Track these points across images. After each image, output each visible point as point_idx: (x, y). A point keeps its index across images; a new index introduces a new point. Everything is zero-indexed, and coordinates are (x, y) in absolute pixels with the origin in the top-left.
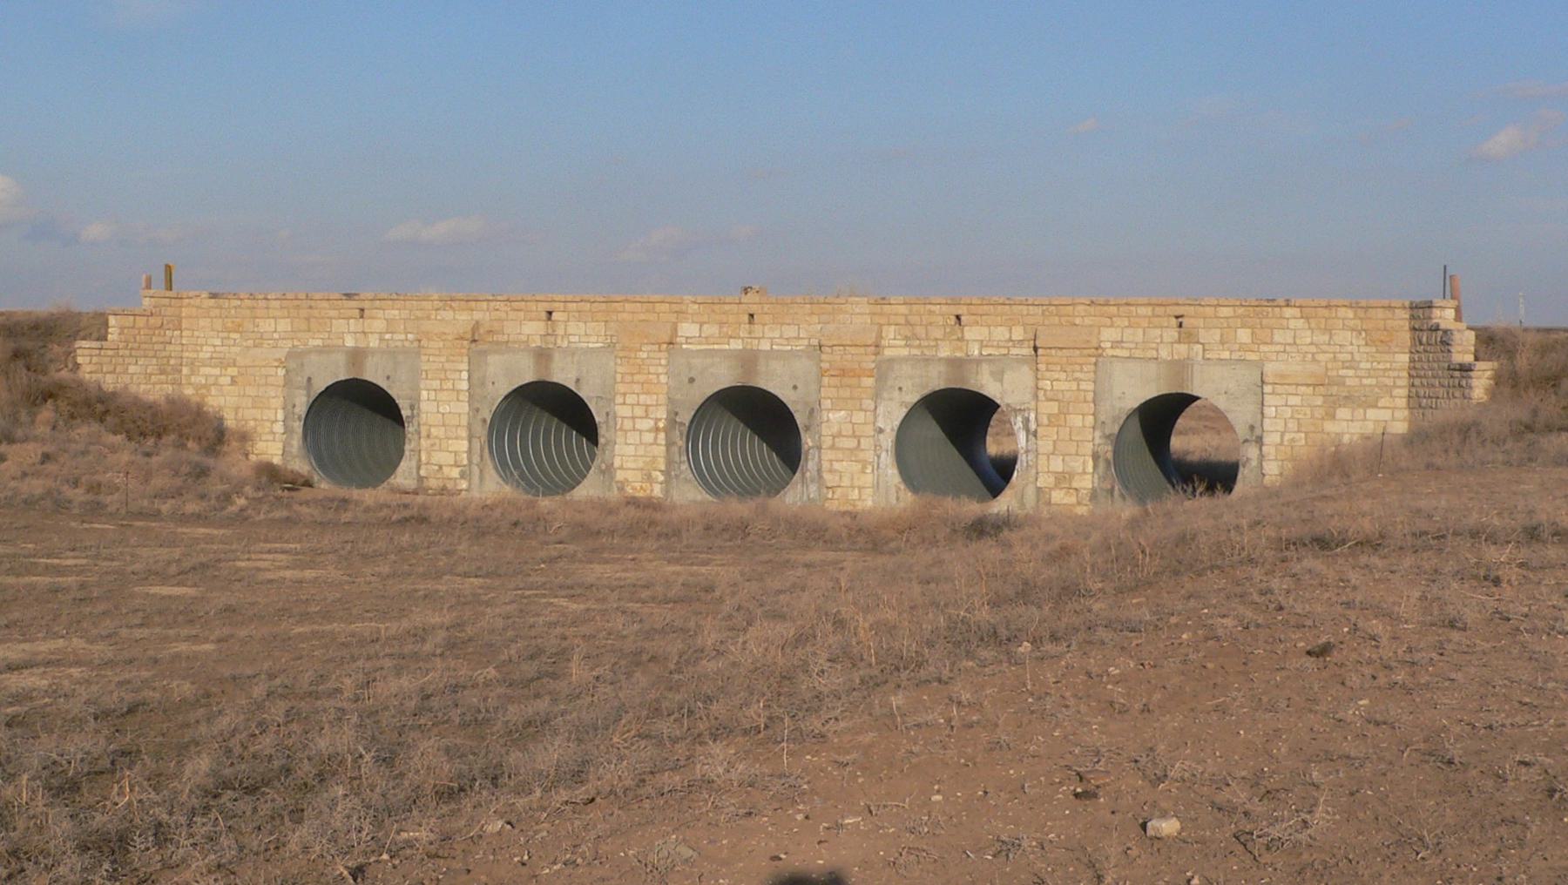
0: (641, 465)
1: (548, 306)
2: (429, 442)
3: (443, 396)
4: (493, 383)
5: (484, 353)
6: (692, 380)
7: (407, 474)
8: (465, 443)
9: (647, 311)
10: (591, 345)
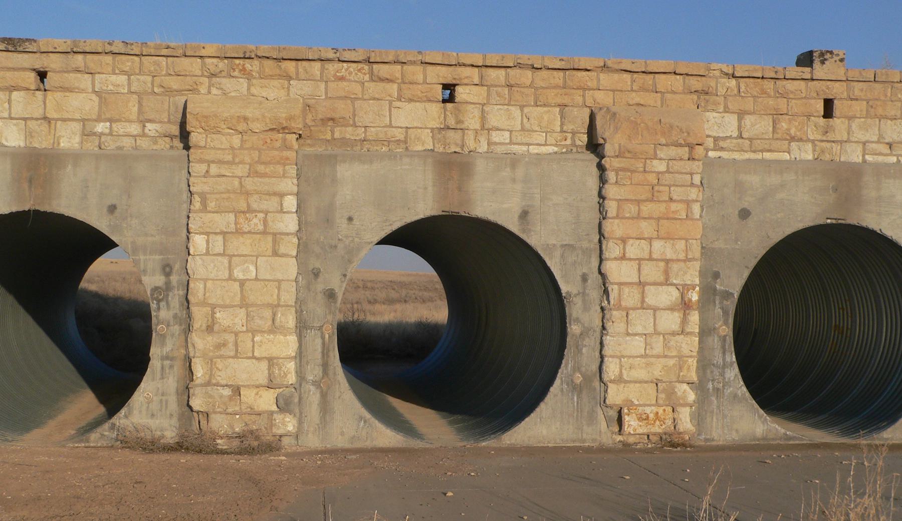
0: (657, 373)
1: (446, 75)
2: (211, 340)
3: (242, 245)
4: (350, 219)
5: (331, 160)
6: (745, 214)
7: (154, 406)
8: (293, 339)
9: (643, 89)
10: (534, 150)
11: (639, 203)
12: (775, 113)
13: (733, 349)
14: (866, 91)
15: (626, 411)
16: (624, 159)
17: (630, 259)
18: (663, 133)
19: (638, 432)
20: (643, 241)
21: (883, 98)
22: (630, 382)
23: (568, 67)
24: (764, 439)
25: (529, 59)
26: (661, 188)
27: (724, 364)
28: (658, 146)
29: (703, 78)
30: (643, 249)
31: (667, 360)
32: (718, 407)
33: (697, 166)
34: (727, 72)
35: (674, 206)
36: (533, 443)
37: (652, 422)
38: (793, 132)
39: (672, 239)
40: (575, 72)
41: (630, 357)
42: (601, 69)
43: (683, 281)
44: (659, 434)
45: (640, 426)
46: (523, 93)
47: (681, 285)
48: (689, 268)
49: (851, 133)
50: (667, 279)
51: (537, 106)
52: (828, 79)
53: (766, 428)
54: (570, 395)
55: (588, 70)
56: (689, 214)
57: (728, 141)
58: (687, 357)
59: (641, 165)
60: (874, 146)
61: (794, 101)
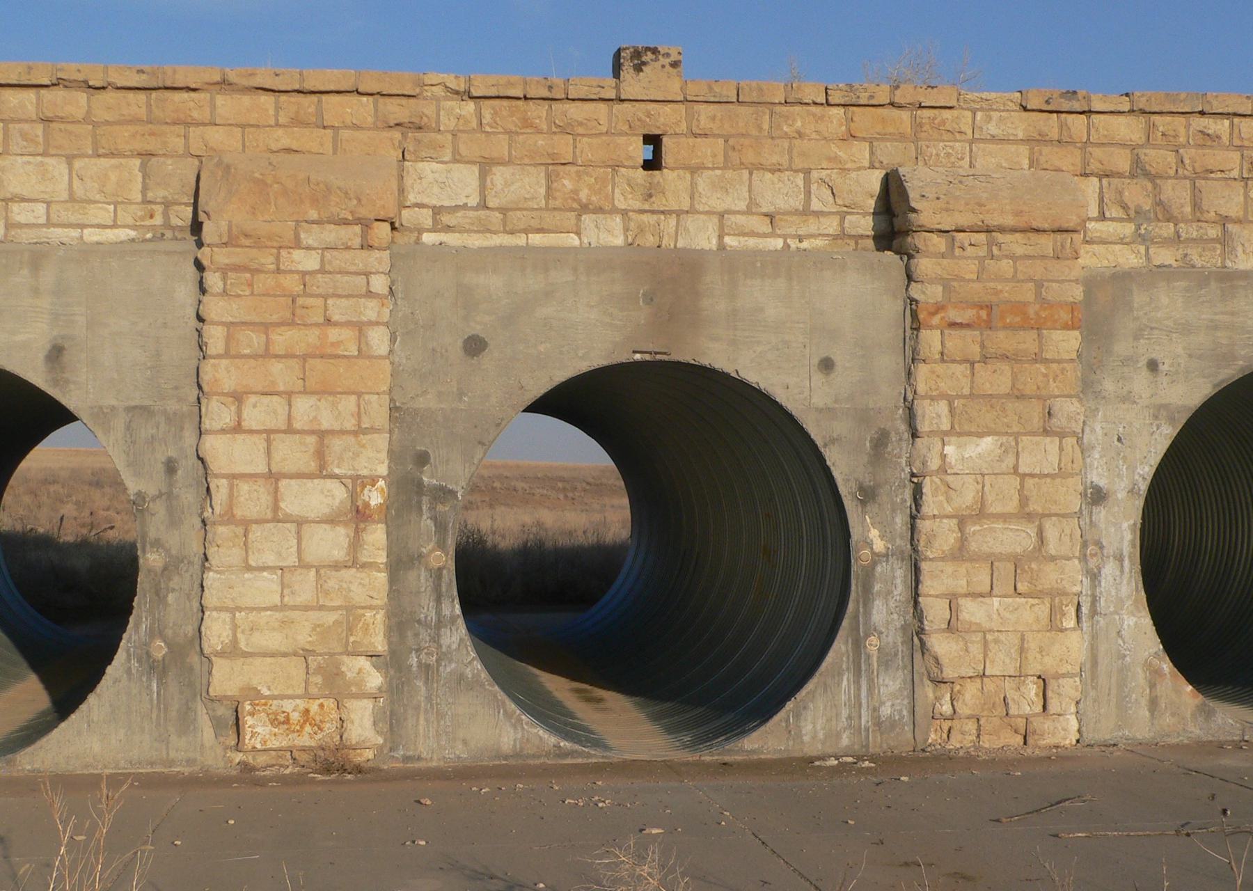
0: (304, 637)
6: (475, 346)
9: (297, 122)
10: (91, 235)
11: (267, 328)
12: (550, 161)
13: (455, 593)
14: (721, 120)
15: (248, 707)
16: (238, 250)
17: (251, 432)
18: (315, 201)
19: (269, 745)
20: (275, 398)
21: (754, 132)
22: (251, 655)
23: (155, 85)
24: (517, 755)
25: (79, 71)
26: (310, 301)
27: (439, 621)
28: (304, 224)
29: (412, 101)
30: (275, 412)
31: (323, 613)
32: (429, 699)
33: (378, 260)
34: (457, 88)
35: (334, 334)
36: (76, 767)
37: (298, 728)
38: (583, 195)
39: (331, 394)
40: (168, 94)
41: (252, 609)
42: (218, 87)
43: (354, 469)
44: (311, 749)
45: (275, 735)
46: (71, 133)
47: (351, 477)
48: (363, 446)
49: (697, 195)
50: (322, 467)
51: (99, 156)
52: (648, 98)
53: (519, 736)
54: (144, 679)
55: (194, 90)
56: (364, 348)
57: (459, 214)
58: (363, 608)
59: (271, 259)
60: (740, 219)
61: (585, 139)
